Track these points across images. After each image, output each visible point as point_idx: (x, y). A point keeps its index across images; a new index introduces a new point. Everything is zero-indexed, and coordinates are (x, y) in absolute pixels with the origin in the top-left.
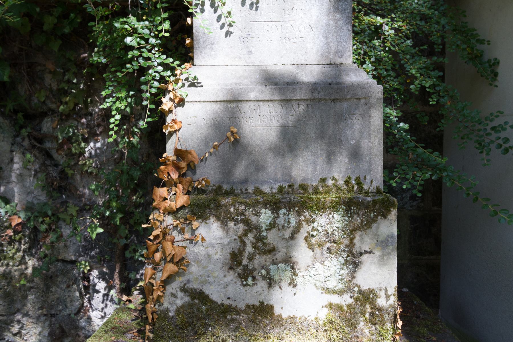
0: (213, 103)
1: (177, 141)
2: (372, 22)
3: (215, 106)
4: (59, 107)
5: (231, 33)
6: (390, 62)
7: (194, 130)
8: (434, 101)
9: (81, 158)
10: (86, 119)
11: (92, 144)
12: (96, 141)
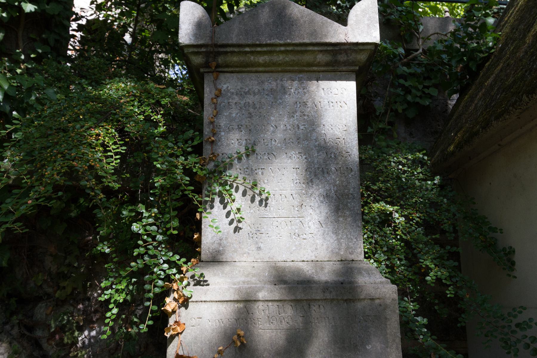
0: (219, 303)
1: (179, 345)
2: (382, 210)
3: (221, 306)
4: (55, 292)
5: (240, 229)
6: (402, 251)
7: (198, 332)
8: (452, 294)
9: (72, 349)
10: (83, 305)
11: (86, 333)
12: (91, 330)
